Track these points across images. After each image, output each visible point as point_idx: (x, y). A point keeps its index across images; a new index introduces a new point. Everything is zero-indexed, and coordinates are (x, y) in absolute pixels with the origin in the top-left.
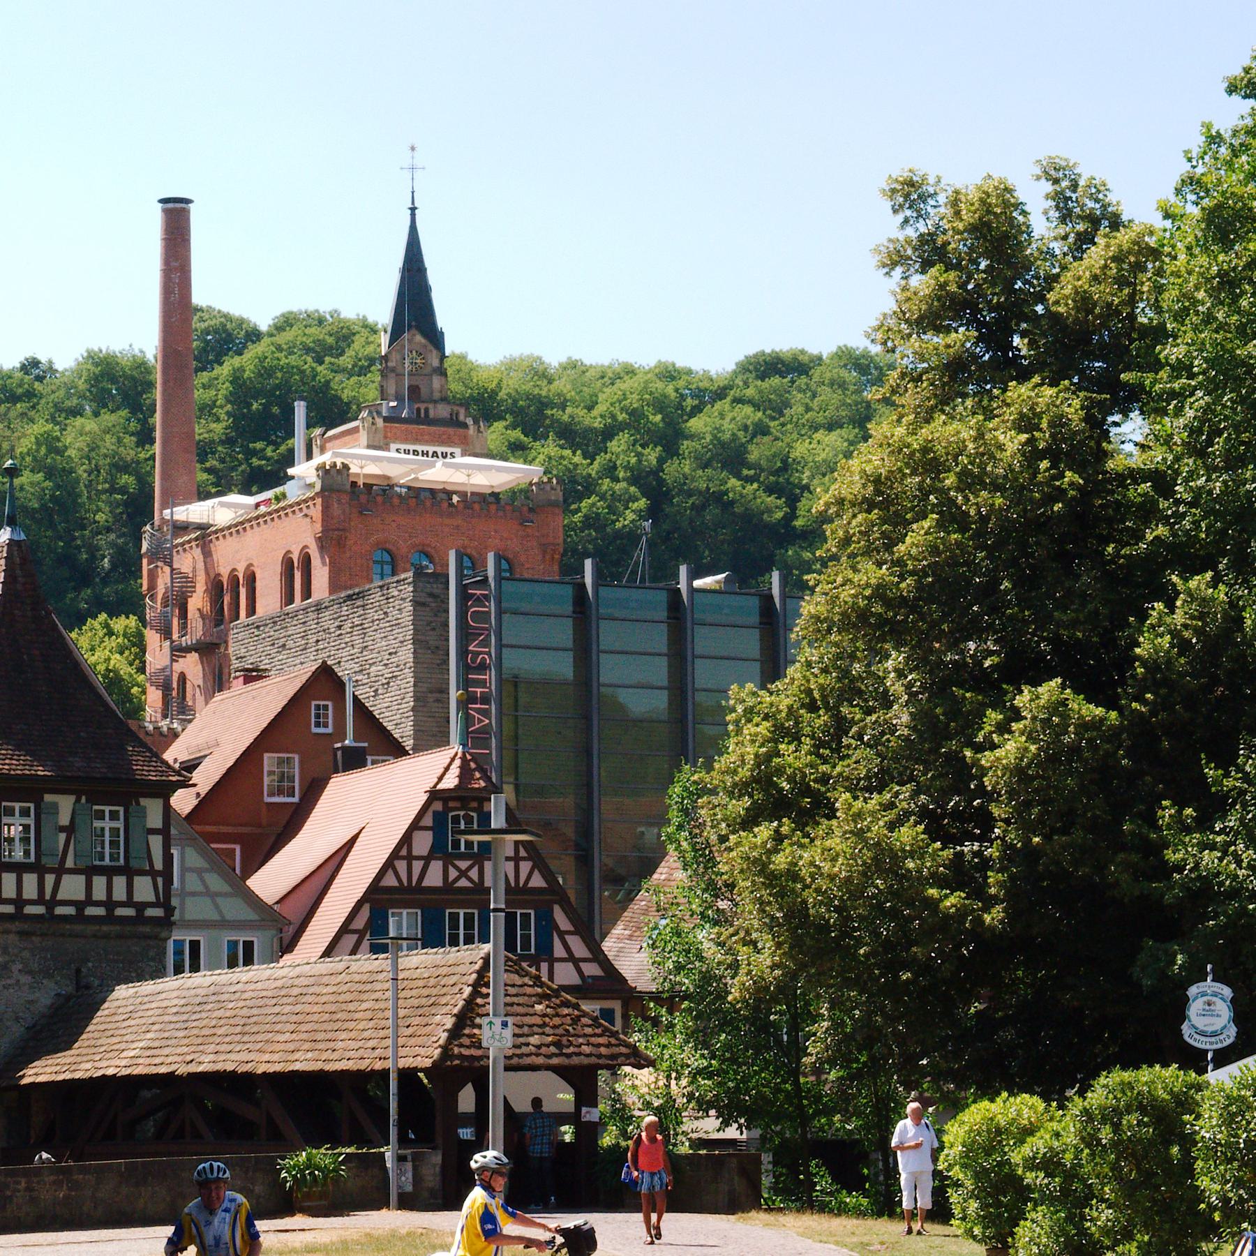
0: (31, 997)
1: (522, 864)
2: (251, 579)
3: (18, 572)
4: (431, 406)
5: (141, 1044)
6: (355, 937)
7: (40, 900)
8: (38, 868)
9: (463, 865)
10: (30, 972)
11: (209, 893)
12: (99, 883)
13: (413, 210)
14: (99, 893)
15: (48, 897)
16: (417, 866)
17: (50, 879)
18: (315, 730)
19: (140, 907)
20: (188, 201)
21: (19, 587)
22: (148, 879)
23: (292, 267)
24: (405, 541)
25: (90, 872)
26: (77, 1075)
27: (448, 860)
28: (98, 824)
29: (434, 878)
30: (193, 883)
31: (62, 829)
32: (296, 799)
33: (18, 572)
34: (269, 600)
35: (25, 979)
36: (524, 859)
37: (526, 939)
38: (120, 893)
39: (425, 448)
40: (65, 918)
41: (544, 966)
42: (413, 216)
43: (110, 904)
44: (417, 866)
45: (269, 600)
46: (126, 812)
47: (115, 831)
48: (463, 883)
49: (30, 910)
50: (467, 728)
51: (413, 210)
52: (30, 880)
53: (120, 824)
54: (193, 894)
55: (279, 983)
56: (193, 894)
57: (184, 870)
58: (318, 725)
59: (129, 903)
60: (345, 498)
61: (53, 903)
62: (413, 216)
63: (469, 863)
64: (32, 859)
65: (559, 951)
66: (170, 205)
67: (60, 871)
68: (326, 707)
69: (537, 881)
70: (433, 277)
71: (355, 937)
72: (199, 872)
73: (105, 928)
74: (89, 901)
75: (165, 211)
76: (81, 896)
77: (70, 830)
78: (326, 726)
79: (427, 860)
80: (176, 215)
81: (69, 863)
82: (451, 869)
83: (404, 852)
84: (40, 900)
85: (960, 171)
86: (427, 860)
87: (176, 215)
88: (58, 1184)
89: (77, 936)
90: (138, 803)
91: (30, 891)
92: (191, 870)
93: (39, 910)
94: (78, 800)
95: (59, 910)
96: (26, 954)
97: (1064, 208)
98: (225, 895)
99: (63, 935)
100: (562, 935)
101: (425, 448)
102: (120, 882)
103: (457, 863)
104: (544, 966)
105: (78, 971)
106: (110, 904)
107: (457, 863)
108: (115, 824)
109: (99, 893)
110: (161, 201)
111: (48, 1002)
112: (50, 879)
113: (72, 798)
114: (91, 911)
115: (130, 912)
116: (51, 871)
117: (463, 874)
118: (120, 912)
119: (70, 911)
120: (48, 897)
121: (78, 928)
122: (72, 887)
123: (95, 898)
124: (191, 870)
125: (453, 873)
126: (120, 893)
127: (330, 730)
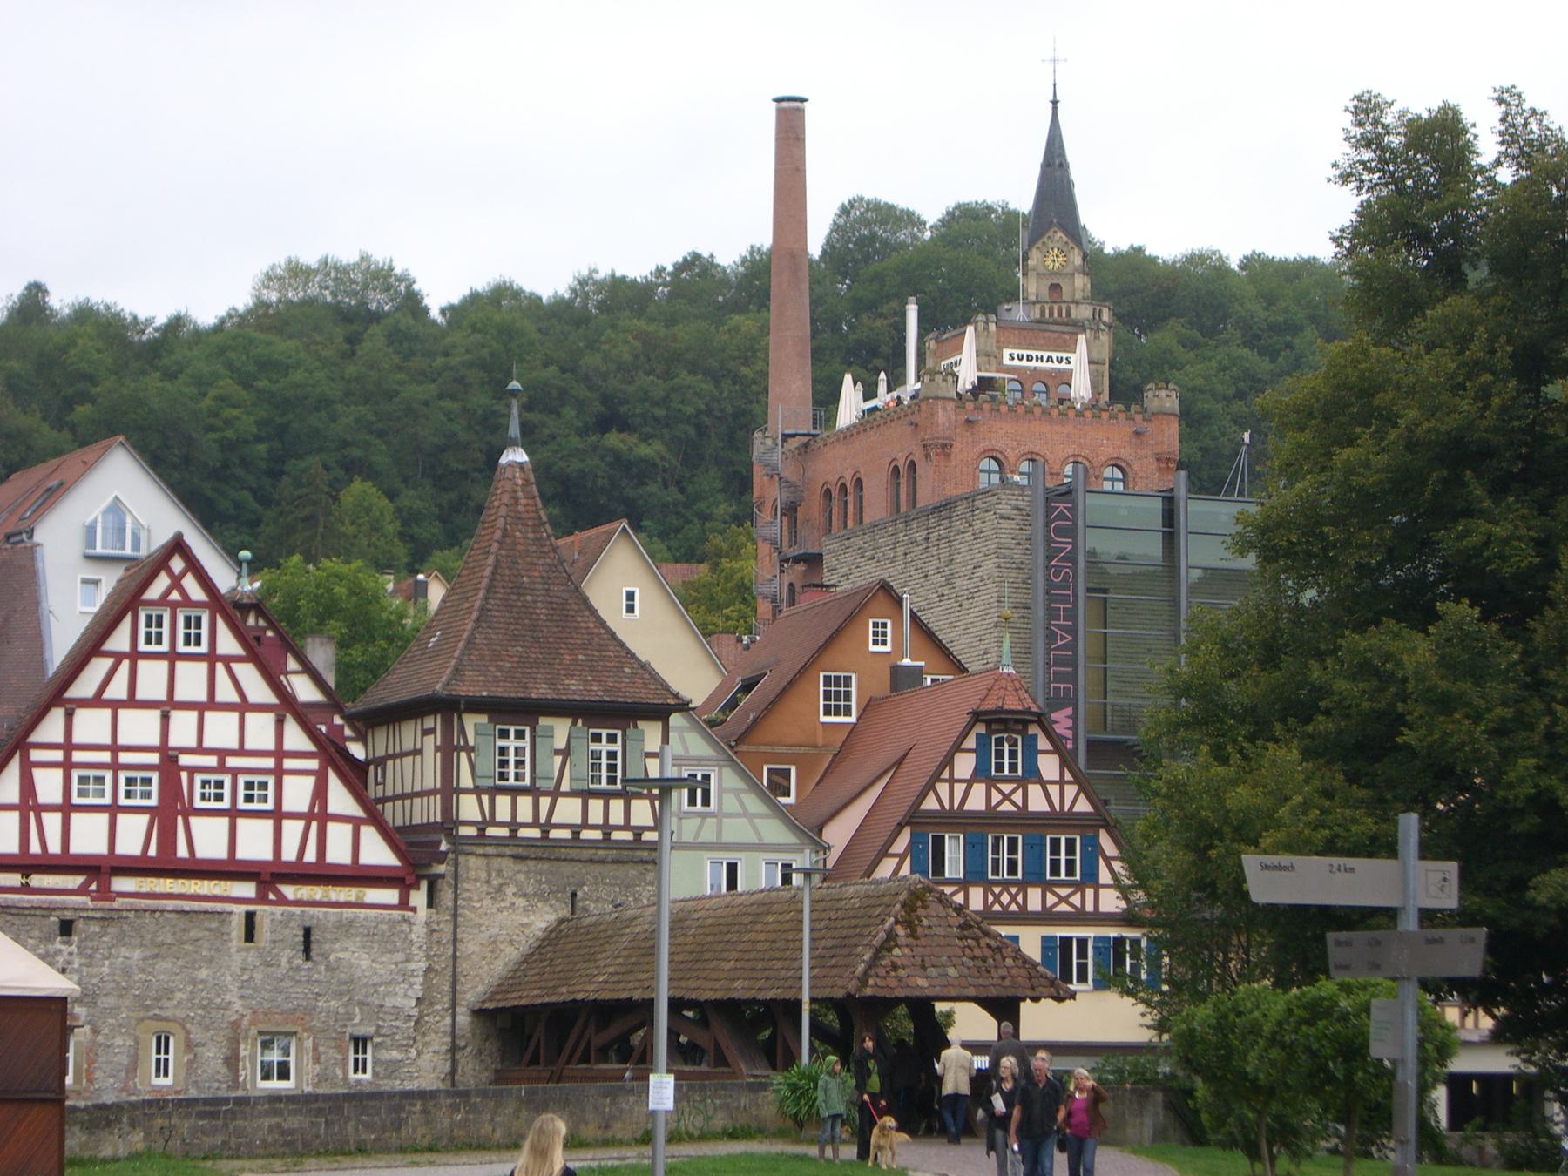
0: (525, 920)
1: (1067, 787)
2: (859, 484)
3: (520, 494)
4: (1073, 306)
5: (611, 970)
6: (896, 860)
7: (535, 824)
8: (534, 791)
9: (1007, 788)
10: (525, 895)
11: (745, 814)
12: (596, 806)
13: (1055, 102)
14: (596, 816)
15: (542, 821)
16: (959, 789)
17: (545, 802)
18: (873, 648)
19: (638, 831)
20: (803, 100)
21: (520, 508)
22: (647, 802)
23: (932, 160)
24: (1013, 449)
25: (586, 795)
26: (554, 999)
27: (991, 783)
28: (594, 747)
29: (976, 802)
30: (731, 804)
31: (557, 752)
32: (853, 719)
33: (520, 494)
34: (876, 505)
35: (521, 902)
36: (1069, 782)
37: (1070, 865)
38: (616, 817)
39: (1040, 354)
40: (560, 843)
41: (1090, 892)
42: (1055, 109)
43: (607, 828)
44: (959, 789)
45: (876, 505)
46: (624, 735)
47: (612, 755)
48: (1007, 807)
49: (524, 833)
50: (1049, 644)
51: (1055, 102)
52: (525, 803)
53: (617, 747)
54: (731, 815)
55: (736, 911)
56: (731, 815)
57: (721, 791)
58: (875, 642)
59: (626, 826)
60: (951, 406)
61: (547, 827)
62: (1055, 109)
63: (1013, 786)
64: (527, 782)
65: (1105, 876)
66: (785, 104)
67: (555, 794)
68: (884, 625)
69: (1083, 806)
70: (1076, 173)
71: (896, 860)
72: (736, 792)
73: (601, 852)
74: (585, 825)
75: (780, 112)
76: (577, 819)
77: (566, 753)
78: (884, 643)
79: (970, 783)
80: (790, 120)
81: (565, 787)
82: (994, 793)
83: (946, 775)
84: (535, 824)
85: (1415, 98)
86: (970, 783)
87: (790, 120)
88: (455, 1108)
89: (573, 860)
90: (636, 726)
91: (525, 814)
92: (728, 791)
93: (535, 833)
94: (574, 723)
95: (555, 834)
96: (521, 877)
97: (1510, 135)
98: (762, 816)
99: (557, 859)
100: (1107, 860)
101: (1040, 354)
102: (617, 806)
103: (1000, 786)
104: (1090, 892)
105: (574, 895)
106: (607, 828)
107: (1000, 786)
108: (612, 747)
109: (596, 816)
110: (778, 100)
111: (544, 925)
112: (545, 802)
113: (569, 721)
114: (586, 834)
115: (627, 836)
116: (546, 794)
117: (1007, 797)
118: (616, 835)
119: (566, 834)
120: (542, 821)
121: (573, 853)
122: (568, 810)
123: (590, 822)
124: (728, 791)
125: (996, 797)
126: (616, 817)
127: (888, 648)
